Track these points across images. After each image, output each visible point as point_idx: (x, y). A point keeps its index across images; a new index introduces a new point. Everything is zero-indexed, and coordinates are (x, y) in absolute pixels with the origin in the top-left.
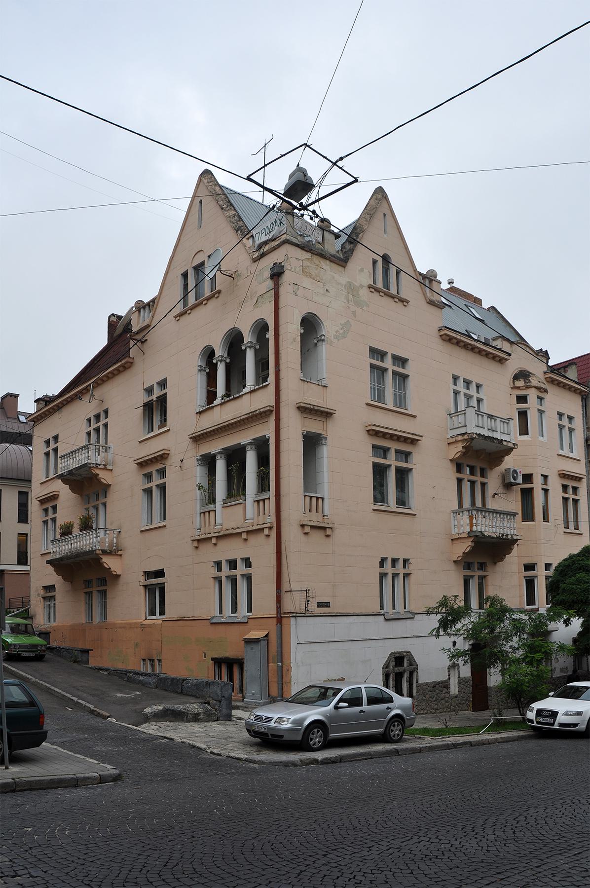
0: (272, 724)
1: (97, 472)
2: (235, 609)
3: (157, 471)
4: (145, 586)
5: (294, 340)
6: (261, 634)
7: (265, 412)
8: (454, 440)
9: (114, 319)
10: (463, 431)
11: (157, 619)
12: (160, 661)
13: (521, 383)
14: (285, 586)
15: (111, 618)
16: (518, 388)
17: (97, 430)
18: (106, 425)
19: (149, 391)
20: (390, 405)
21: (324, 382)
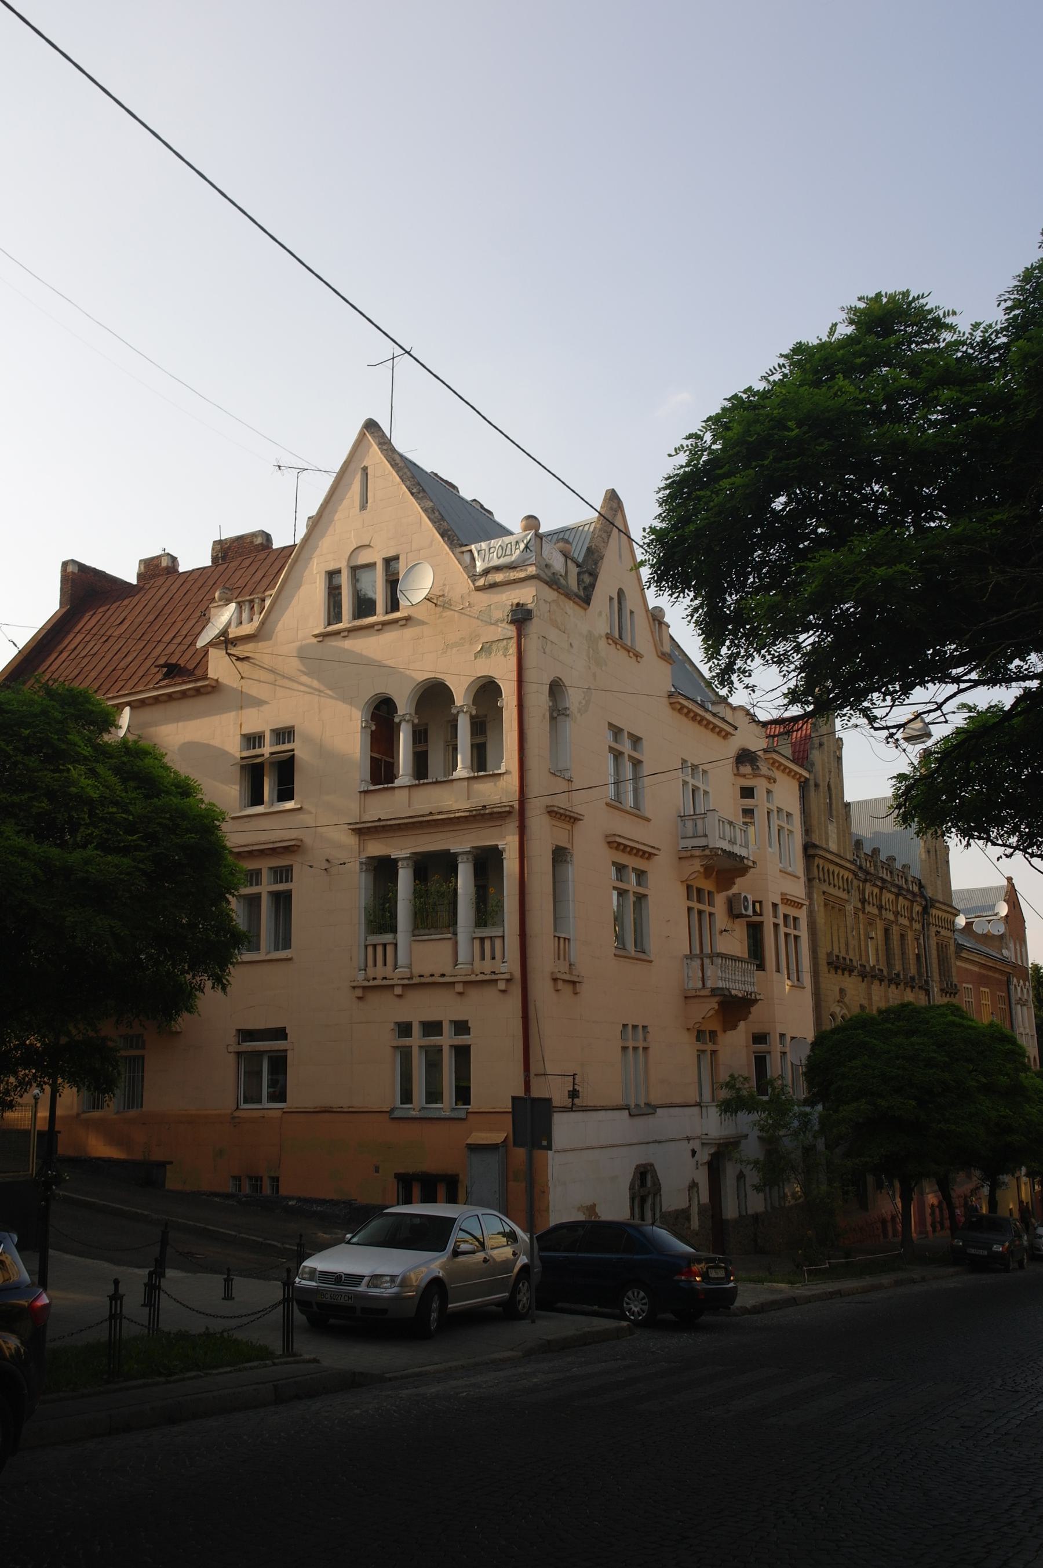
0: (362, 1288)
2: (434, 1095)
3: (271, 868)
5: (544, 715)
8: (689, 854)
9: (70, 569)
10: (702, 842)
13: (746, 769)
14: (533, 1070)
16: (744, 776)
19: (253, 740)
21: (567, 775)
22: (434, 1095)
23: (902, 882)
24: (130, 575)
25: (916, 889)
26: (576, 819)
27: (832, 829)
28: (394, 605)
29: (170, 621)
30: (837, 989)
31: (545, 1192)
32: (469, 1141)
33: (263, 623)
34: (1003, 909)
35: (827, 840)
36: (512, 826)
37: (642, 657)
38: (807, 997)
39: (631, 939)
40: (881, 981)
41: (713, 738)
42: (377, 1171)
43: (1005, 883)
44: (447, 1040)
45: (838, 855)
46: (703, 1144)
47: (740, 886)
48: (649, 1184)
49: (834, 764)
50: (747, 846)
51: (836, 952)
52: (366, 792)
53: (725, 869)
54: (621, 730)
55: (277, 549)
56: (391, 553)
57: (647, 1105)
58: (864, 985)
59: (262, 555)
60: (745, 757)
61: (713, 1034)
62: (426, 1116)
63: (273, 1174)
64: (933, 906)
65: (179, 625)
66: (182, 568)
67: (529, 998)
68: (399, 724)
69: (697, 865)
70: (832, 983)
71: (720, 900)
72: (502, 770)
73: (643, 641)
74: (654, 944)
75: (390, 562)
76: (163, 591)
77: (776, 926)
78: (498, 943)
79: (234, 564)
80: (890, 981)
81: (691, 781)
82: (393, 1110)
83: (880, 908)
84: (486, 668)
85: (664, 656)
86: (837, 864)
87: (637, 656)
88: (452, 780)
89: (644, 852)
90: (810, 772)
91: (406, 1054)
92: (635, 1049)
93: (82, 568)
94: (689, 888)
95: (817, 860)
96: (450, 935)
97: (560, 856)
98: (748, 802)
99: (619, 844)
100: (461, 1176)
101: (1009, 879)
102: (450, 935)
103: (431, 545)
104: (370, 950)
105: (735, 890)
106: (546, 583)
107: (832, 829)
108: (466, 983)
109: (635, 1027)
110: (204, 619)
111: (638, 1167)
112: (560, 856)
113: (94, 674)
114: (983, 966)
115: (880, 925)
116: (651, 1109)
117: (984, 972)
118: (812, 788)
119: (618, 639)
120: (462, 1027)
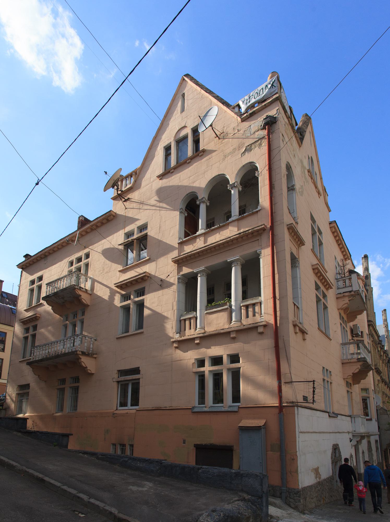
1: (80, 293)
2: (218, 398)
4: (118, 382)
6: (261, 423)
7: (258, 231)
8: (342, 295)
9: (81, 218)
10: (350, 289)
11: (130, 409)
12: (132, 446)
15: (81, 409)
17: (79, 269)
18: (87, 265)
22: (218, 398)
31: (294, 459)
32: (241, 425)
42: (184, 443)
48: (337, 455)
62: (213, 410)
63: (130, 443)
67: (279, 335)
78: (257, 308)
82: (194, 408)
100: (235, 447)
104: (183, 322)
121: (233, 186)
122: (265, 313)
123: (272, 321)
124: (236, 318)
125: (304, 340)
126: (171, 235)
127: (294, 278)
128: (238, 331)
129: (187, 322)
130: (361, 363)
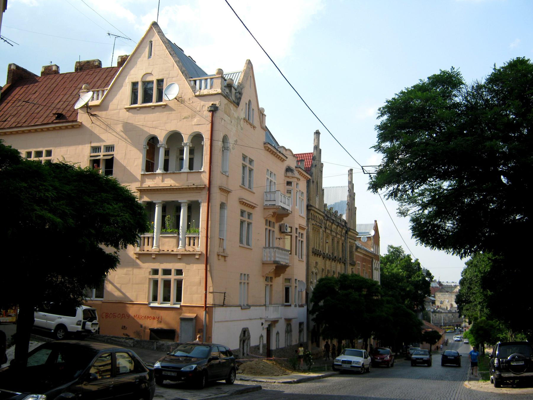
9: (12, 67)
10: (273, 203)
13: (289, 174)
20: (247, 188)
23: (339, 221)
24: (38, 72)
25: (344, 224)
26: (229, 192)
27: (317, 199)
28: (160, 99)
29: (57, 94)
30: (315, 262)
32: (181, 317)
33: (103, 101)
34: (373, 233)
35: (315, 203)
36: (205, 194)
37: (256, 127)
38: (304, 266)
39: (245, 239)
40: (330, 259)
41: (278, 162)
43: (374, 222)
44: (160, 277)
45: (319, 210)
46: (266, 321)
47: (286, 221)
48: (246, 335)
49: (108, 70)
50: (289, 205)
51: (315, 248)
52: (143, 174)
53: (281, 214)
54: (246, 157)
55: (105, 68)
56: (160, 78)
57: (247, 305)
58: (323, 261)
59: (98, 70)
60: (289, 169)
61: (271, 278)
64: (349, 231)
65: (61, 96)
66: (61, 72)
68: (159, 148)
69: (271, 212)
70: (314, 259)
71: (277, 226)
72: (202, 170)
73: (256, 123)
74: (253, 242)
75: (160, 82)
76: (53, 81)
77: (296, 237)
79: (86, 72)
80: (333, 259)
81: (270, 178)
83: (331, 231)
84: (197, 129)
85: (262, 128)
86: (318, 213)
87: (254, 127)
88: (181, 173)
89: (252, 206)
90: (311, 176)
91: (156, 282)
92: (244, 283)
93: (18, 67)
94: (266, 220)
95: (311, 211)
96: (176, 235)
97: (222, 206)
98: (289, 187)
99: (244, 202)
101: (376, 221)
102: (176, 235)
103: (177, 76)
105: (282, 222)
106: (224, 97)
107: (317, 199)
108: (182, 255)
109: (245, 275)
110: (77, 98)
111: (243, 329)
112: (222, 206)
113: (23, 114)
114: (364, 255)
115: (331, 237)
116: (249, 306)
117: (364, 257)
118: (311, 183)
119: (247, 120)
120: (179, 272)
121: (186, 144)
122: (200, 247)
123: (204, 252)
124: (182, 244)
125: (225, 261)
126: (135, 164)
127: (222, 216)
128: (183, 255)
129: (146, 240)
130: (276, 265)
